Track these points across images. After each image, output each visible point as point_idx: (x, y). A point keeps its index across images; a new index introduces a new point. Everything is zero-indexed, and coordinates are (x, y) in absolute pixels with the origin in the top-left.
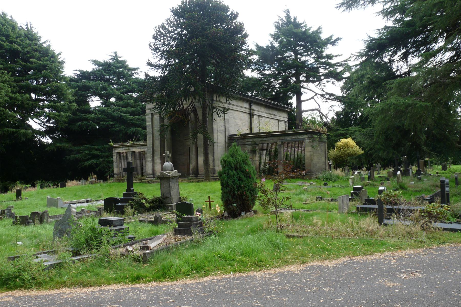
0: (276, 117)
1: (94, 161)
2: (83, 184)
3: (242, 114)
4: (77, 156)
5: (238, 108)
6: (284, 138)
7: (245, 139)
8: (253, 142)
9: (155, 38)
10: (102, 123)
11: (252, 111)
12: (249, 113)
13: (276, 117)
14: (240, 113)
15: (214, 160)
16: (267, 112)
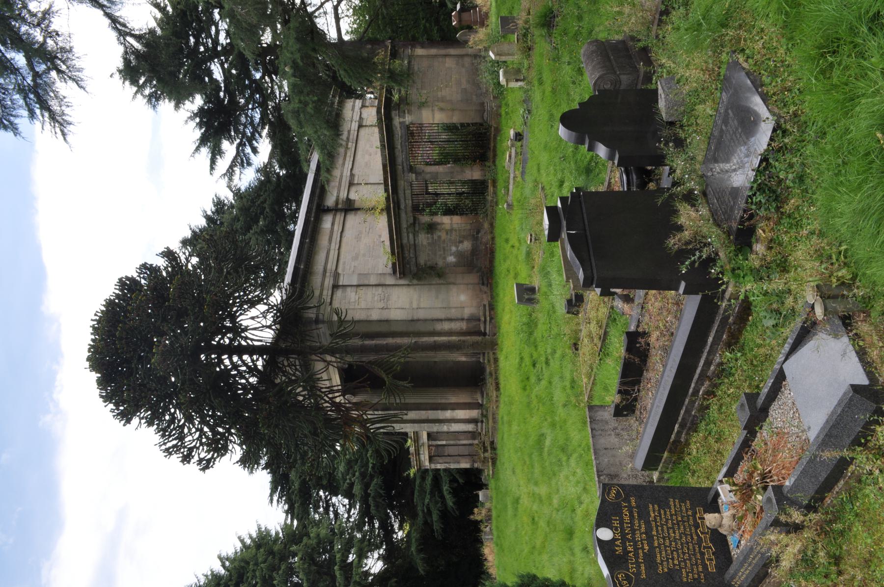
0: (352, 132)
1: (445, 488)
2: (490, 537)
3: (348, 234)
4: (435, 517)
5: (334, 246)
6: (400, 167)
7: (402, 244)
8: (409, 230)
9: (186, 459)
10: (370, 469)
11: (340, 206)
12: (343, 214)
13: (353, 134)
14: (344, 240)
15: (450, 320)
16: (340, 161)
